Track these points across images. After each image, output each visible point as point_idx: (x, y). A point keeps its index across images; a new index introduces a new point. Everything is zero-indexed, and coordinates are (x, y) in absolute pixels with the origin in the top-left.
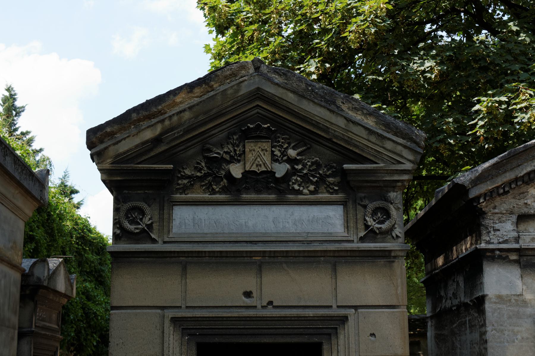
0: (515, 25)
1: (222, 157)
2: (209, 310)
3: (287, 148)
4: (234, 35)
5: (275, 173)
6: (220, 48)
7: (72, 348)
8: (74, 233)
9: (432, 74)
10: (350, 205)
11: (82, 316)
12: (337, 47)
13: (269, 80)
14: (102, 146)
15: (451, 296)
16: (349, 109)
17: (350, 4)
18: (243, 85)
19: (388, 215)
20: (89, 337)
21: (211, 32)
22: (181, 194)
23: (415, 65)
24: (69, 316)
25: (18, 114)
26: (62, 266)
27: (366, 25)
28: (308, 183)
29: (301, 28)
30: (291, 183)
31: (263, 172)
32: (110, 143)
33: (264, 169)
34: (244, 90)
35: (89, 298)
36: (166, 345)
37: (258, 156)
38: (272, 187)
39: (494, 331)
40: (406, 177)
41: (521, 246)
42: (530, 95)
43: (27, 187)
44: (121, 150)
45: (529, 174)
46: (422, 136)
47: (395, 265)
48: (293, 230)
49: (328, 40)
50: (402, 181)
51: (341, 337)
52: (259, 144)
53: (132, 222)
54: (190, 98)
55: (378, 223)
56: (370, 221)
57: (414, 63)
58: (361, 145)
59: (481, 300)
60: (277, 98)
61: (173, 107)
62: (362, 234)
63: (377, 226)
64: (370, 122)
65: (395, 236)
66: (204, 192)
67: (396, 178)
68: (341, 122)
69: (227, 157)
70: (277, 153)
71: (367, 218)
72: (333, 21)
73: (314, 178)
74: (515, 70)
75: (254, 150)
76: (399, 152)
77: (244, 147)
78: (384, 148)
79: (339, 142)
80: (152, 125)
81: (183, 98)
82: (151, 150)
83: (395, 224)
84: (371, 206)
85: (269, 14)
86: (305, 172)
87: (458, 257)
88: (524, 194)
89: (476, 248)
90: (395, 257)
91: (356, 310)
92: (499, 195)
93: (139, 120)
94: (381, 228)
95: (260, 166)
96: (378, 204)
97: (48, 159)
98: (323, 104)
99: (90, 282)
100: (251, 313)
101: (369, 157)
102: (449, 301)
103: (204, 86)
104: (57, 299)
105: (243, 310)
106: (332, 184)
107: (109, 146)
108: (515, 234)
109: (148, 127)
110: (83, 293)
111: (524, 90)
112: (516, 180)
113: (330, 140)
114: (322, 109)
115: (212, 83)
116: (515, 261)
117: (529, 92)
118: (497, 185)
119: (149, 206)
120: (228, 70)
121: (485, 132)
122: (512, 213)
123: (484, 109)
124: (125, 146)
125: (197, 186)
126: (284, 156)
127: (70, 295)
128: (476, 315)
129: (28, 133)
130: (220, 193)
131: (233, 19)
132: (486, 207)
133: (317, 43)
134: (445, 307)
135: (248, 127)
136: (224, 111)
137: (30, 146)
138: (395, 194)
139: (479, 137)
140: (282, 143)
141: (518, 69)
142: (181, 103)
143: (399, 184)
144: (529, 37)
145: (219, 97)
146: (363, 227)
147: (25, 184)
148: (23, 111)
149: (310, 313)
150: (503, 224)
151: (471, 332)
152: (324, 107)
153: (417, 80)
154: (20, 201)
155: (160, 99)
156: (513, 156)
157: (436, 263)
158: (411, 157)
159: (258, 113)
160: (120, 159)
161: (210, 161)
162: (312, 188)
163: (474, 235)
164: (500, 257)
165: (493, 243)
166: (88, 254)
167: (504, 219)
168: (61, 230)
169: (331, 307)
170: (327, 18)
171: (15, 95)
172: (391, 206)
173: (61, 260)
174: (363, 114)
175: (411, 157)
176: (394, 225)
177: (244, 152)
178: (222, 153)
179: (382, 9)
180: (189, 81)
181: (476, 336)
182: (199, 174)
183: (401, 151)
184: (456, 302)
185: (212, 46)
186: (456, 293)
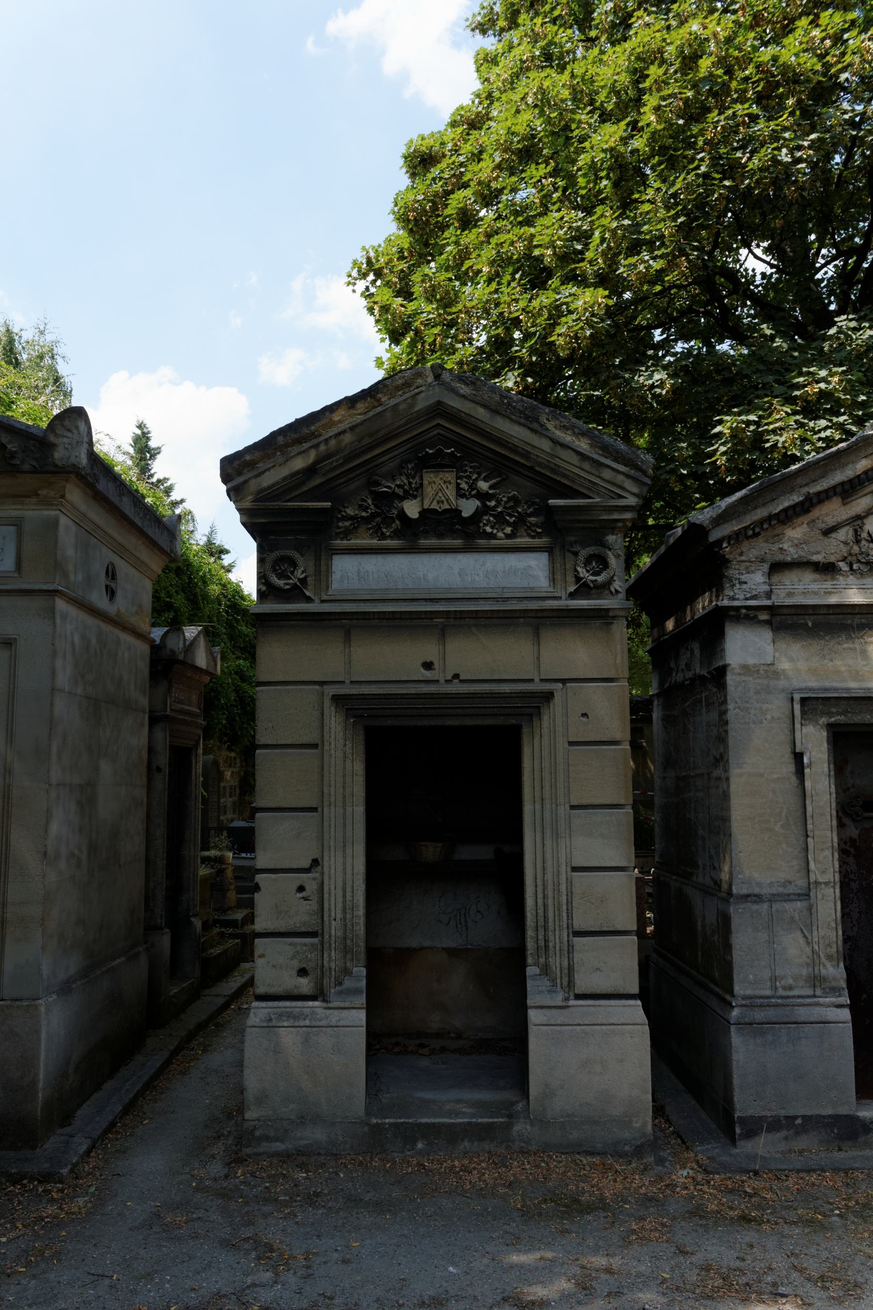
0: (768, 328)
1: (394, 492)
2: (380, 686)
3: (476, 480)
4: (413, 344)
5: (461, 511)
6: (395, 361)
7: (225, 739)
8: (223, 599)
9: (663, 389)
10: (557, 552)
11: (235, 700)
12: (542, 355)
13: (453, 390)
14: (241, 479)
15: (683, 667)
16: (555, 427)
17: (560, 299)
18: (420, 397)
19: (605, 565)
20: (245, 726)
21: (383, 340)
22: (342, 539)
23: (642, 378)
24: (219, 700)
25: (153, 457)
26: (202, 636)
27: (580, 326)
28: (503, 523)
29: (497, 332)
30: (481, 525)
31: (446, 510)
32: (250, 475)
33: (448, 507)
34: (421, 404)
35: (243, 678)
36: (326, 729)
37: (440, 490)
38: (458, 529)
39: (737, 710)
40: (628, 516)
41: (773, 603)
42: (786, 413)
43: (153, 536)
44: (265, 484)
45: (785, 510)
46: (650, 462)
47: (614, 627)
48: (484, 584)
49: (531, 347)
50: (623, 520)
51: (545, 718)
52: (441, 475)
53: (281, 576)
54: (351, 416)
55: (592, 575)
56: (582, 572)
57: (640, 376)
58: (572, 475)
59: (722, 671)
60: (463, 414)
61: (330, 427)
62: (572, 589)
63: (591, 578)
64: (583, 445)
65: (613, 591)
66: (372, 537)
67: (616, 516)
68: (546, 445)
69: (400, 492)
70: (464, 486)
71: (578, 569)
72: (538, 321)
73: (511, 517)
74: (768, 383)
75: (434, 483)
76: (619, 483)
77: (421, 478)
78: (600, 477)
79: (543, 471)
80: (304, 452)
81: (342, 415)
82: (303, 483)
83: (614, 575)
84: (584, 553)
85: (454, 313)
86: (499, 510)
87: (692, 618)
88: (779, 537)
89: (717, 605)
90: (614, 617)
91: (564, 684)
92: (748, 538)
93: (287, 445)
94: (596, 581)
95: (442, 502)
96: (591, 550)
97: (190, 512)
98: (522, 421)
99: (245, 659)
100: (432, 689)
101: (581, 490)
102: (681, 675)
103: (369, 399)
104: (197, 678)
105: (422, 685)
106: (534, 525)
107: (250, 479)
108: (766, 588)
109: (298, 454)
110: (236, 673)
111: (778, 407)
112: (770, 518)
113: (531, 469)
114: (522, 427)
115: (380, 395)
116: (766, 622)
117: (785, 409)
118: (744, 525)
119: (302, 555)
120: (400, 378)
121: (728, 460)
122: (763, 561)
123: (727, 431)
124: (269, 479)
125: (362, 529)
126: (473, 489)
127: (213, 671)
128: (715, 690)
129: (166, 480)
130: (391, 537)
131: (411, 323)
132: (731, 553)
133: (516, 351)
134: (676, 681)
135: (427, 452)
136: (396, 432)
137: (169, 496)
138: (614, 537)
139: (720, 467)
140: (470, 472)
141: (771, 381)
142: (340, 422)
143: (620, 524)
144: (786, 342)
145: (388, 414)
146: (573, 579)
147: (150, 532)
148: (159, 453)
149: (506, 688)
150: (751, 575)
151: (708, 712)
152: (524, 426)
153: (643, 398)
154: (144, 554)
155: (313, 418)
156: (766, 487)
157: (663, 627)
158: (635, 490)
159: (439, 434)
160: (266, 495)
161: (379, 497)
162: (508, 530)
163: (714, 590)
164: (747, 617)
165: (738, 599)
166: (241, 626)
167: (753, 568)
168: (206, 596)
169: (533, 680)
170: (529, 318)
171: (149, 433)
172: (610, 553)
173: (200, 628)
174: (574, 434)
175: (635, 490)
176: (612, 577)
177: (421, 485)
178: (393, 486)
179: (600, 305)
180: (350, 393)
181: (714, 715)
182: (364, 514)
183: (623, 482)
184: (690, 675)
185: (384, 359)
186: (691, 663)
